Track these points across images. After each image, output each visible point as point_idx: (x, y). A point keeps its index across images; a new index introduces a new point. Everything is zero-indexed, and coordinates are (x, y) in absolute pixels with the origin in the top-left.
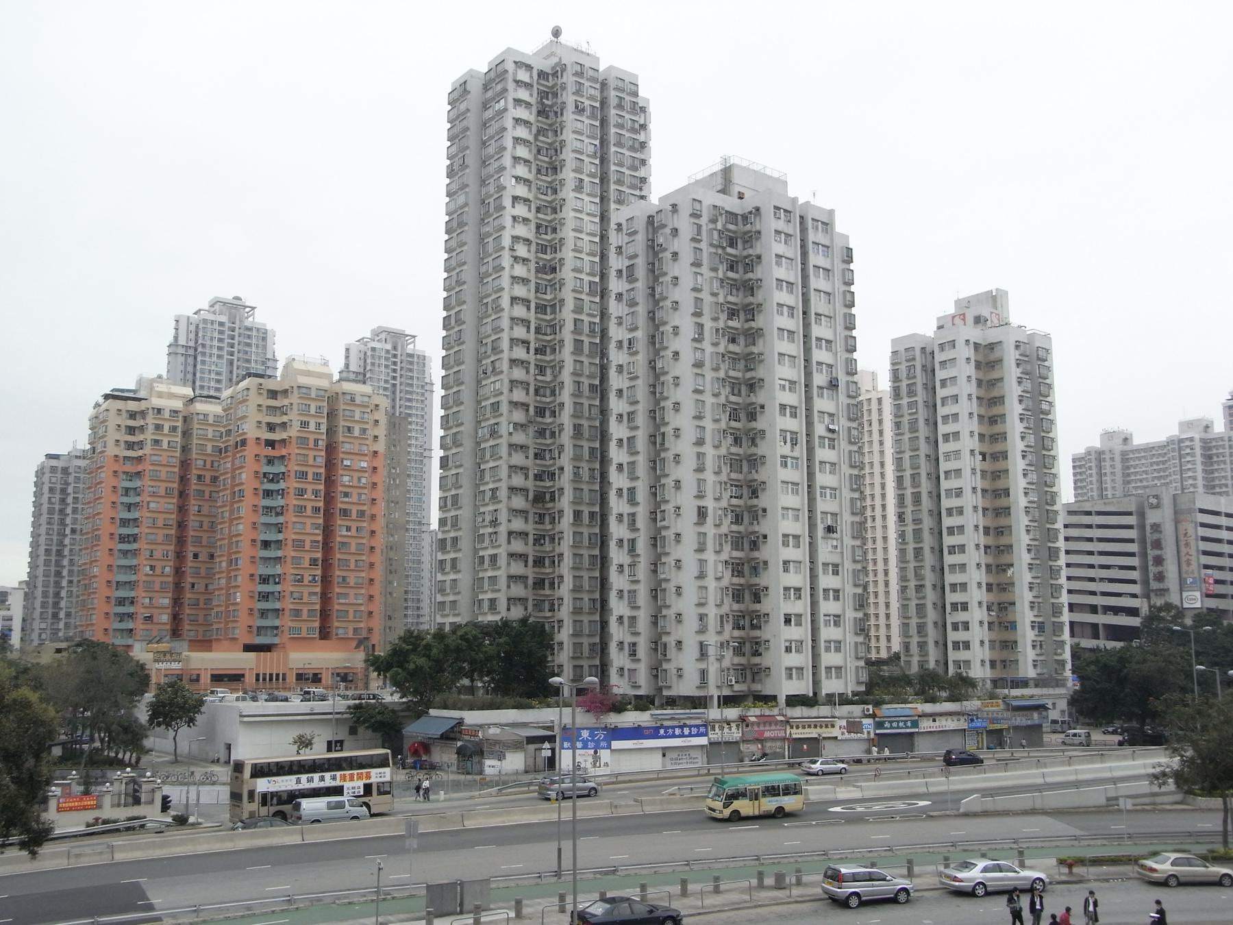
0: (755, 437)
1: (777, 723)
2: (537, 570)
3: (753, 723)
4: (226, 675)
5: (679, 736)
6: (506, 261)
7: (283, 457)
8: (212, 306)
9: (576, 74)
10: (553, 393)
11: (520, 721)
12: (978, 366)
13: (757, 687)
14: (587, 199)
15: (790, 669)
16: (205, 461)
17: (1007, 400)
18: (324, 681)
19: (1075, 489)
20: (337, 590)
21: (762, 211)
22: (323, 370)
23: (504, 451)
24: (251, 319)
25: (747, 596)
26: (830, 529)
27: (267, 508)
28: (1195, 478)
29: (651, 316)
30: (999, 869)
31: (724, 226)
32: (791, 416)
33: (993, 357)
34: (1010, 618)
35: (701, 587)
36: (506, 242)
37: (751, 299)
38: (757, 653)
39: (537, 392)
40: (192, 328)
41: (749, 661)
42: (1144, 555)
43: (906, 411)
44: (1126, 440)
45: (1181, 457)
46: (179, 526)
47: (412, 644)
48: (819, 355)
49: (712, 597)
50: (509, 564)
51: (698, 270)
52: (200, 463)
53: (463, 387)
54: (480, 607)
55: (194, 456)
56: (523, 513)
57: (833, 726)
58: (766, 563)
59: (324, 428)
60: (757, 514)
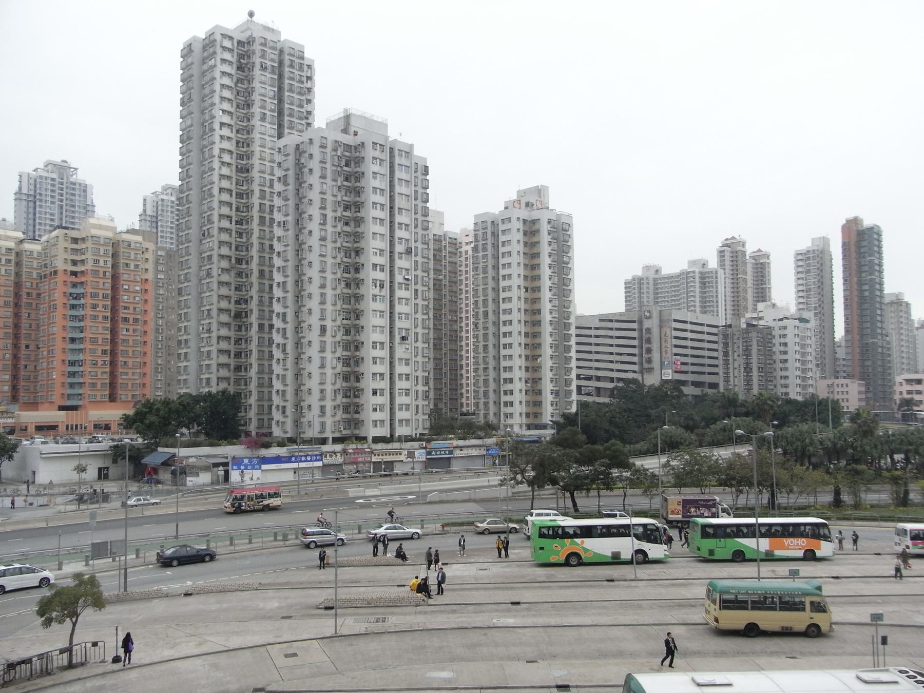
0: (359, 283)
1: (365, 453)
2: (236, 360)
3: (350, 453)
4: (45, 426)
5: (304, 461)
6: (216, 164)
7: (82, 283)
8: (46, 166)
9: (262, 44)
10: (247, 250)
11: (212, 454)
12: (525, 233)
13: (357, 432)
14: (269, 126)
15: (376, 421)
16: (32, 283)
17: (541, 255)
18: (112, 429)
19: (626, 302)
20: (121, 370)
22: (111, 224)
23: (215, 286)
24: (74, 177)
25: (352, 378)
27: (73, 316)
29: (297, 207)
30: (395, 528)
33: (534, 228)
34: (539, 388)
35: (322, 374)
36: (216, 152)
37: (358, 199)
38: (356, 396)
39: (237, 249)
40: (32, 181)
42: (641, 347)
43: (481, 260)
44: (657, 271)
45: (687, 283)
46: (15, 327)
47: (149, 408)
48: (399, 233)
49: (329, 379)
50: (218, 357)
51: (324, 181)
52: (28, 284)
53: (190, 244)
54: (201, 383)
55: (24, 280)
56: (227, 325)
57: (400, 454)
58: (363, 359)
59: (109, 265)
60: (359, 329)
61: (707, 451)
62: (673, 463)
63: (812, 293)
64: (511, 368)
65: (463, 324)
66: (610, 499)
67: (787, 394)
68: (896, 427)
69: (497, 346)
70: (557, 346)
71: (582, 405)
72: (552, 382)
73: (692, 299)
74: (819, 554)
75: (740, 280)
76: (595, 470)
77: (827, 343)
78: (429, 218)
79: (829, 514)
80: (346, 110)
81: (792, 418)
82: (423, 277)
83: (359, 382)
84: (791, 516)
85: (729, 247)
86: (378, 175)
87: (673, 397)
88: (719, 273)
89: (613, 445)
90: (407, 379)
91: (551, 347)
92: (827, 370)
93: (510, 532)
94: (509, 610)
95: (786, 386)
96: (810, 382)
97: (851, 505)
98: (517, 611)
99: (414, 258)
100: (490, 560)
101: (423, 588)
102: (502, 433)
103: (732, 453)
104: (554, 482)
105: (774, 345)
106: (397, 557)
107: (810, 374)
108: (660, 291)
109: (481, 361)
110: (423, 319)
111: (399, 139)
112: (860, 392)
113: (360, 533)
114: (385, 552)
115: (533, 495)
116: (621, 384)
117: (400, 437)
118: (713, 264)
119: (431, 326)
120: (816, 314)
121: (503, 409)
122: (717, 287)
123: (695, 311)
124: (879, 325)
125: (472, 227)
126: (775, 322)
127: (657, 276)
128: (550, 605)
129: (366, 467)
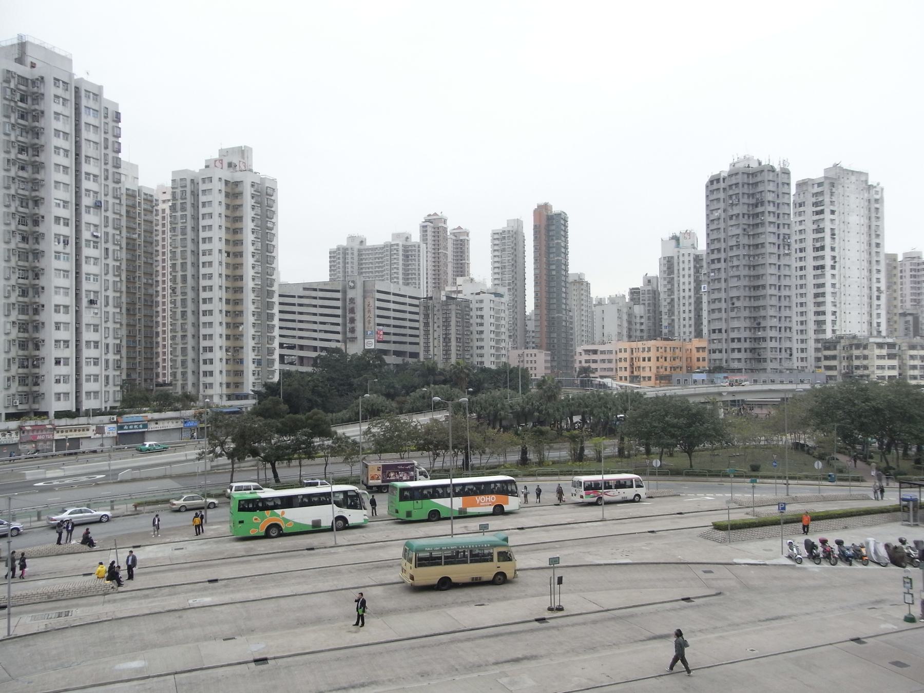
1: (47, 430)
3: (28, 431)
12: (227, 195)
13: (36, 406)
15: (59, 394)
17: (244, 219)
19: (330, 271)
21: (45, 79)
25: (31, 346)
26: (92, 302)
28: (398, 269)
30: (81, 512)
31: (16, 86)
32: (64, 225)
34: (240, 357)
37: (36, 141)
38: (36, 384)
41: (30, 389)
42: (345, 317)
43: (179, 221)
44: (362, 242)
45: (391, 255)
48: (86, 184)
58: (43, 323)
60: (38, 290)
61: (407, 417)
62: (374, 430)
64: (211, 336)
65: (160, 289)
66: (312, 468)
67: (482, 363)
68: (575, 392)
69: (196, 313)
70: (259, 314)
71: (285, 374)
72: (254, 350)
73: (395, 271)
75: (441, 255)
76: (297, 440)
77: (518, 316)
78: (121, 171)
79: (517, 471)
80: (20, 37)
81: (486, 385)
82: (114, 313)
83: (38, 350)
84: (483, 475)
86: (61, 116)
87: (376, 366)
88: (421, 246)
89: (315, 414)
90: (96, 347)
91: (254, 315)
92: (518, 341)
93: (209, 508)
94: (205, 589)
95: (482, 356)
96: (503, 352)
97: (536, 463)
98: (215, 588)
99: (103, 213)
100: (187, 539)
101: (113, 574)
102: (201, 404)
103: (431, 419)
104: (255, 453)
105: (472, 317)
106: (83, 543)
107: (503, 345)
109: (179, 328)
110: (114, 281)
111: (85, 79)
112: (546, 361)
113: (39, 520)
114: (69, 539)
115: (233, 468)
116: (324, 354)
117: (87, 411)
118: (416, 238)
119: (124, 289)
120: (509, 290)
121: (203, 379)
122: (419, 261)
123: (398, 283)
124: (564, 301)
125: (169, 184)
126: (473, 296)
127: (362, 247)
128: (249, 579)
129: (47, 446)
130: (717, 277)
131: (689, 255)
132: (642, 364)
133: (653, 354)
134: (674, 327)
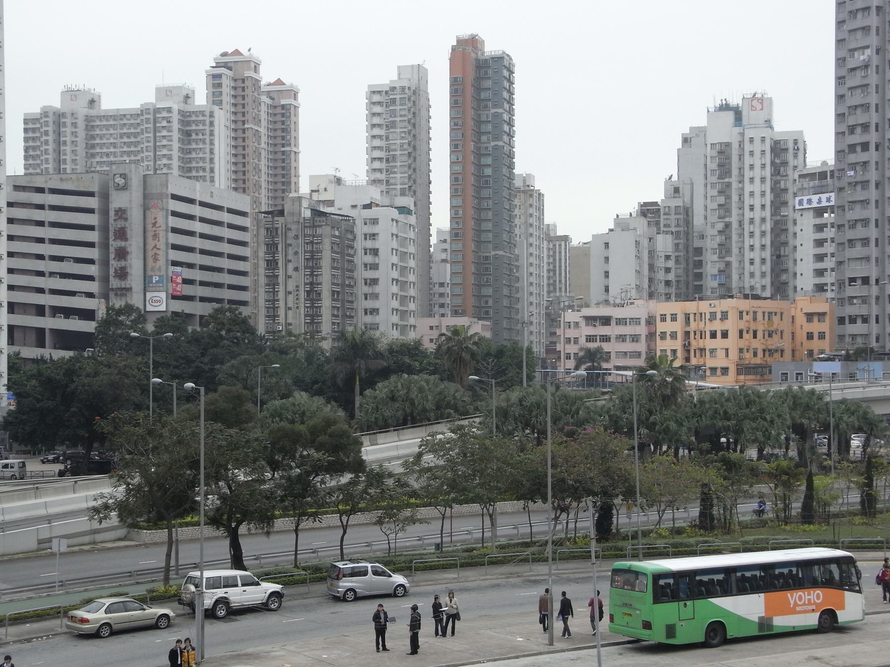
28: (170, 158)
42: (105, 246)
45: (155, 130)
63: (398, 164)
74: (843, 617)
75: (249, 134)
85: (230, 69)
108: (98, 141)
122: (212, 143)
127: (93, 112)
130: (859, 179)
131: (763, 139)
132: (709, 343)
133: (732, 325)
134: (729, 277)
